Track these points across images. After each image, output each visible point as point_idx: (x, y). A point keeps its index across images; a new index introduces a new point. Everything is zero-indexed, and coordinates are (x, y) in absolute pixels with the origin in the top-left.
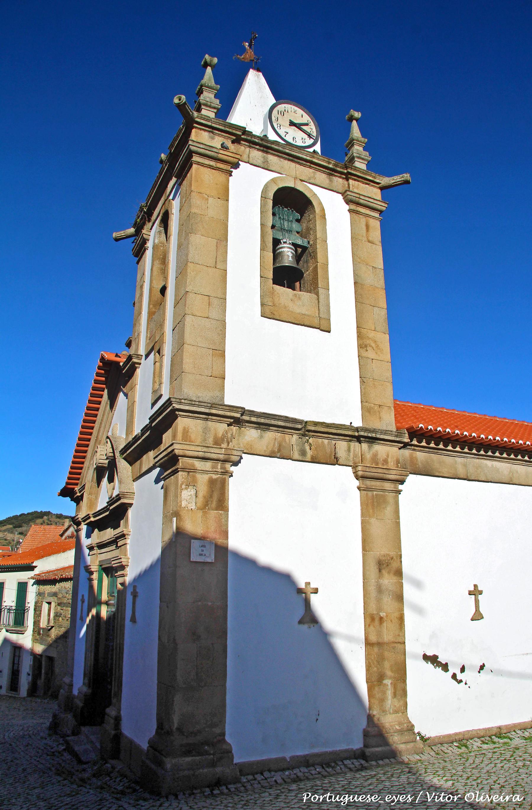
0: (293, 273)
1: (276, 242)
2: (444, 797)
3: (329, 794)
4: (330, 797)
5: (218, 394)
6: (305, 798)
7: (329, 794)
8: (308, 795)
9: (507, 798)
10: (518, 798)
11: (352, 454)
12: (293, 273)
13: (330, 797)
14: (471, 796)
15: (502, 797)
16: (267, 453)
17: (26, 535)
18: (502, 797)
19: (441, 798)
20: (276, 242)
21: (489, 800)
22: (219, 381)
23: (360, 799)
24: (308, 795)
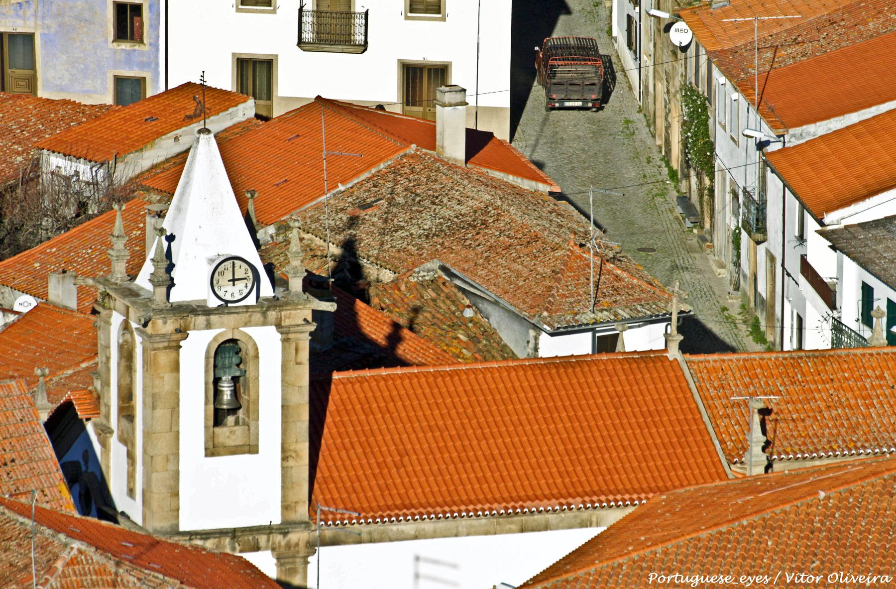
0: (229, 407)
1: (217, 381)
2: (805, 578)
3: (677, 575)
4: (679, 578)
5: (174, 522)
6: (651, 579)
7: (677, 575)
8: (654, 576)
9: (875, 579)
10: (886, 579)
11: (270, 543)
12: (229, 407)
13: (679, 578)
14: (834, 576)
15: (868, 578)
16: (286, 446)
17: (164, 217)
18: (868, 578)
19: (802, 579)
20: (217, 381)
21: (854, 581)
22: (175, 513)
23: (712, 580)
24: (654, 576)
